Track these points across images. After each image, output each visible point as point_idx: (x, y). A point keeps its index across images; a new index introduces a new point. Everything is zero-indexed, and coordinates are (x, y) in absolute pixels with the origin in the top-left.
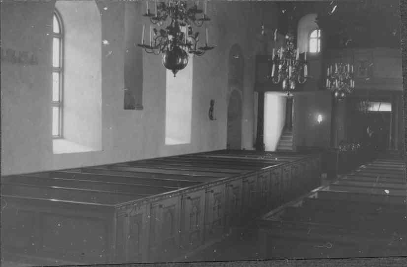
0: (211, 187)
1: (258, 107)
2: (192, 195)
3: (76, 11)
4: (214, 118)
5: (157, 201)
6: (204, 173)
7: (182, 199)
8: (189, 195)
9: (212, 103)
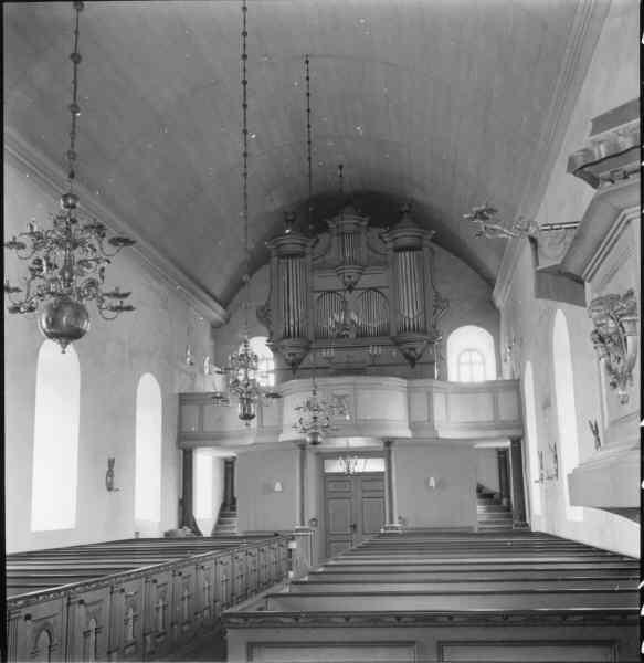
0: (120, 582)
1: (31, 485)
2: (88, 597)
3: (466, 216)
4: (115, 487)
5: (22, 607)
6: (493, 584)
7: (69, 604)
8: (82, 596)
9: (111, 463)
